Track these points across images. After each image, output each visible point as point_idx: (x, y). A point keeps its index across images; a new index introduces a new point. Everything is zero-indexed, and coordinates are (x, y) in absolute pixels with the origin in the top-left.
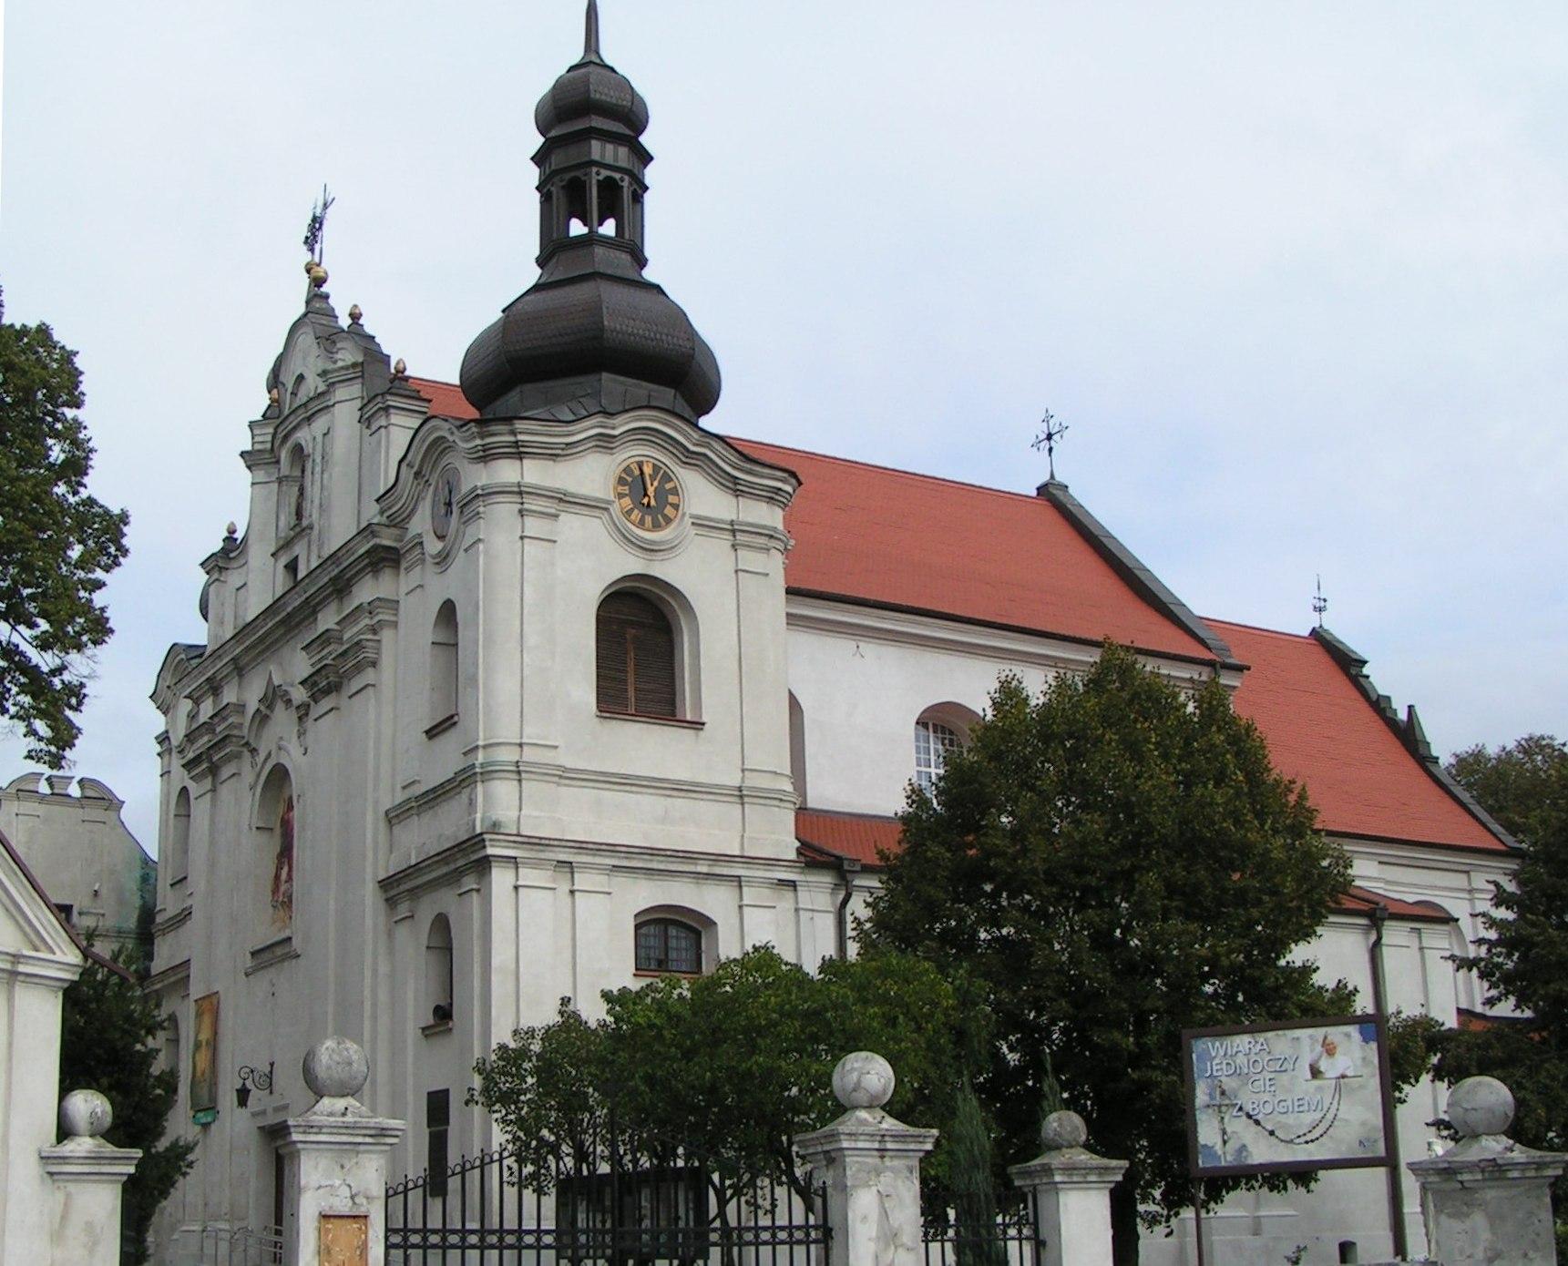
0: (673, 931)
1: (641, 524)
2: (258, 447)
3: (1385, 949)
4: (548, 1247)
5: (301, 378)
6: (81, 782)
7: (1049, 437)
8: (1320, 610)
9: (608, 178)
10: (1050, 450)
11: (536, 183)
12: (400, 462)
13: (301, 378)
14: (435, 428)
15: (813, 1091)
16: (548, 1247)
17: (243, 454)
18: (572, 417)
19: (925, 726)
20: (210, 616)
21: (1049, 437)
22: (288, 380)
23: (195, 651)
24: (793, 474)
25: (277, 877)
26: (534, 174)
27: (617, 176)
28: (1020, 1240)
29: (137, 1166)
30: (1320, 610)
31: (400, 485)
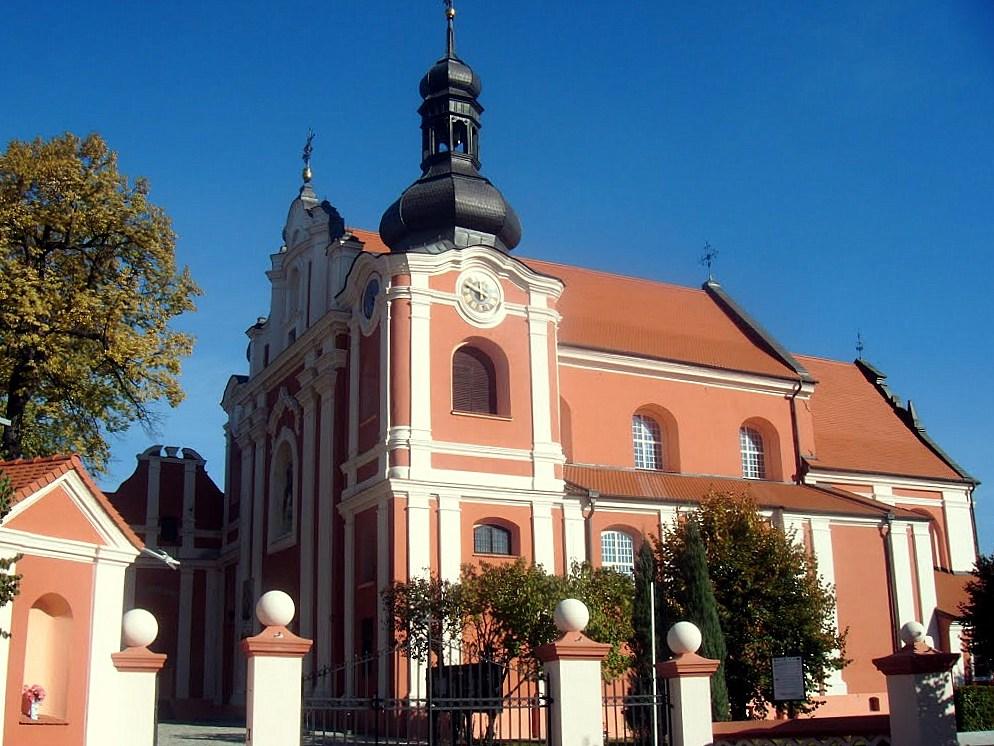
0: (495, 532)
1: (477, 309)
2: (275, 269)
3: (893, 536)
4: (413, 700)
5: (297, 232)
6: (166, 449)
7: (709, 257)
8: (860, 349)
9: (459, 121)
10: (709, 265)
11: (420, 125)
12: (347, 276)
13: (297, 232)
14: (366, 258)
15: (420, 617)
16: (413, 700)
17: (267, 273)
18: (438, 251)
19: (639, 416)
20: (251, 358)
21: (709, 257)
22: (291, 233)
23: (242, 379)
24: (561, 281)
25: (285, 502)
26: (419, 119)
27: (464, 119)
28: (615, 697)
29: (164, 664)
30: (860, 349)
31: (346, 291)
